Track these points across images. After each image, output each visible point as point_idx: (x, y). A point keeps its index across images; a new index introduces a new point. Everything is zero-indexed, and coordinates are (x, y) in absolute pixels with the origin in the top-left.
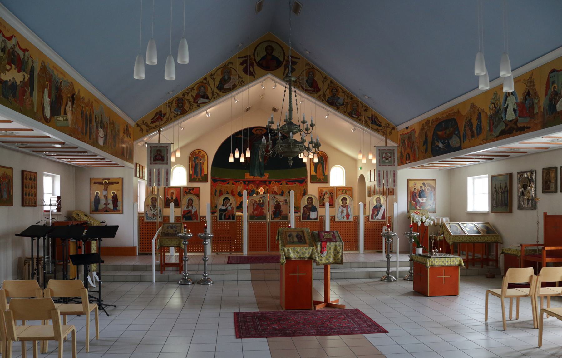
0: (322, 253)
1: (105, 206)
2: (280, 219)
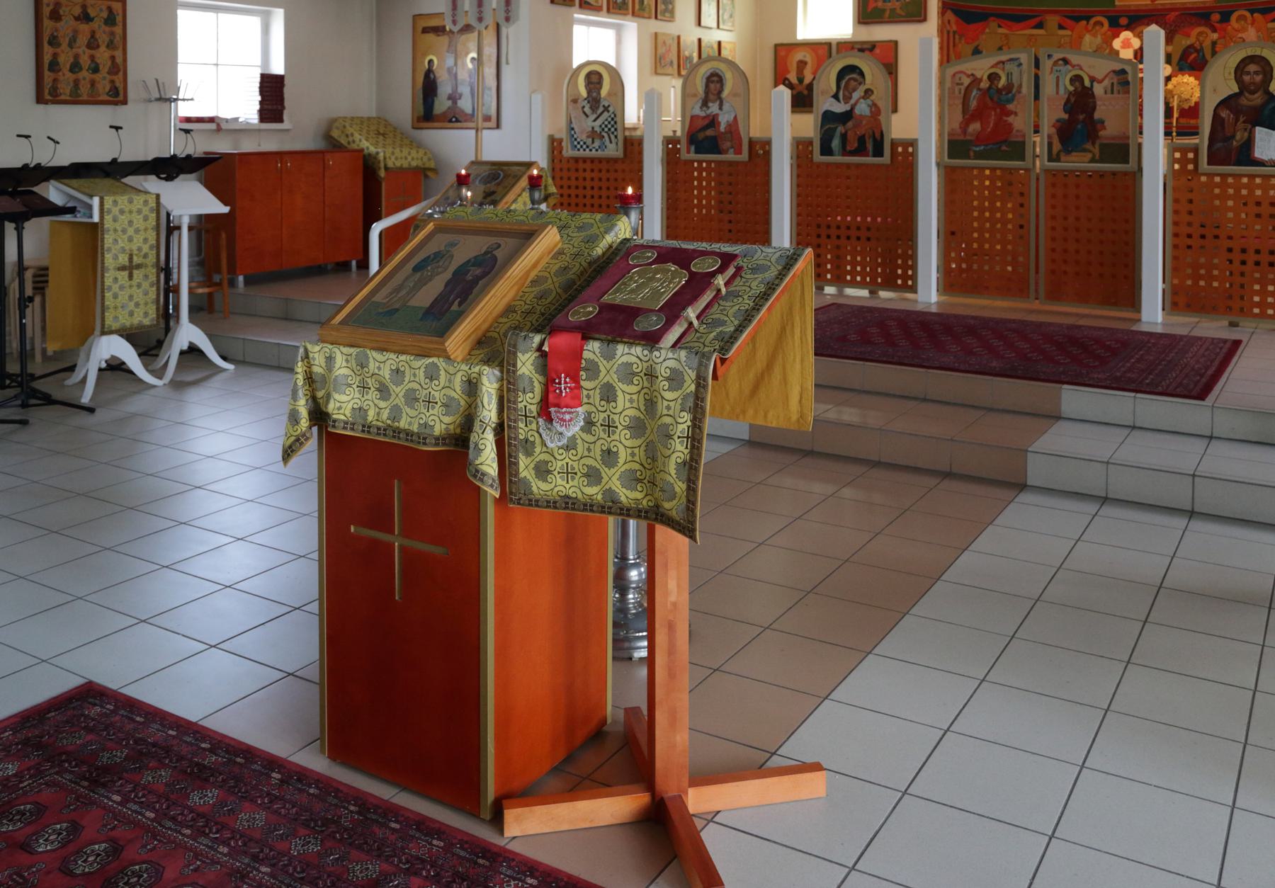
0: (550, 420)
1: (449, 103)
2: (1092, 161)
